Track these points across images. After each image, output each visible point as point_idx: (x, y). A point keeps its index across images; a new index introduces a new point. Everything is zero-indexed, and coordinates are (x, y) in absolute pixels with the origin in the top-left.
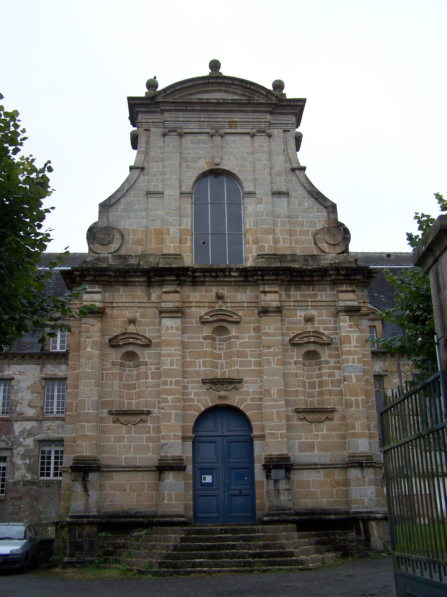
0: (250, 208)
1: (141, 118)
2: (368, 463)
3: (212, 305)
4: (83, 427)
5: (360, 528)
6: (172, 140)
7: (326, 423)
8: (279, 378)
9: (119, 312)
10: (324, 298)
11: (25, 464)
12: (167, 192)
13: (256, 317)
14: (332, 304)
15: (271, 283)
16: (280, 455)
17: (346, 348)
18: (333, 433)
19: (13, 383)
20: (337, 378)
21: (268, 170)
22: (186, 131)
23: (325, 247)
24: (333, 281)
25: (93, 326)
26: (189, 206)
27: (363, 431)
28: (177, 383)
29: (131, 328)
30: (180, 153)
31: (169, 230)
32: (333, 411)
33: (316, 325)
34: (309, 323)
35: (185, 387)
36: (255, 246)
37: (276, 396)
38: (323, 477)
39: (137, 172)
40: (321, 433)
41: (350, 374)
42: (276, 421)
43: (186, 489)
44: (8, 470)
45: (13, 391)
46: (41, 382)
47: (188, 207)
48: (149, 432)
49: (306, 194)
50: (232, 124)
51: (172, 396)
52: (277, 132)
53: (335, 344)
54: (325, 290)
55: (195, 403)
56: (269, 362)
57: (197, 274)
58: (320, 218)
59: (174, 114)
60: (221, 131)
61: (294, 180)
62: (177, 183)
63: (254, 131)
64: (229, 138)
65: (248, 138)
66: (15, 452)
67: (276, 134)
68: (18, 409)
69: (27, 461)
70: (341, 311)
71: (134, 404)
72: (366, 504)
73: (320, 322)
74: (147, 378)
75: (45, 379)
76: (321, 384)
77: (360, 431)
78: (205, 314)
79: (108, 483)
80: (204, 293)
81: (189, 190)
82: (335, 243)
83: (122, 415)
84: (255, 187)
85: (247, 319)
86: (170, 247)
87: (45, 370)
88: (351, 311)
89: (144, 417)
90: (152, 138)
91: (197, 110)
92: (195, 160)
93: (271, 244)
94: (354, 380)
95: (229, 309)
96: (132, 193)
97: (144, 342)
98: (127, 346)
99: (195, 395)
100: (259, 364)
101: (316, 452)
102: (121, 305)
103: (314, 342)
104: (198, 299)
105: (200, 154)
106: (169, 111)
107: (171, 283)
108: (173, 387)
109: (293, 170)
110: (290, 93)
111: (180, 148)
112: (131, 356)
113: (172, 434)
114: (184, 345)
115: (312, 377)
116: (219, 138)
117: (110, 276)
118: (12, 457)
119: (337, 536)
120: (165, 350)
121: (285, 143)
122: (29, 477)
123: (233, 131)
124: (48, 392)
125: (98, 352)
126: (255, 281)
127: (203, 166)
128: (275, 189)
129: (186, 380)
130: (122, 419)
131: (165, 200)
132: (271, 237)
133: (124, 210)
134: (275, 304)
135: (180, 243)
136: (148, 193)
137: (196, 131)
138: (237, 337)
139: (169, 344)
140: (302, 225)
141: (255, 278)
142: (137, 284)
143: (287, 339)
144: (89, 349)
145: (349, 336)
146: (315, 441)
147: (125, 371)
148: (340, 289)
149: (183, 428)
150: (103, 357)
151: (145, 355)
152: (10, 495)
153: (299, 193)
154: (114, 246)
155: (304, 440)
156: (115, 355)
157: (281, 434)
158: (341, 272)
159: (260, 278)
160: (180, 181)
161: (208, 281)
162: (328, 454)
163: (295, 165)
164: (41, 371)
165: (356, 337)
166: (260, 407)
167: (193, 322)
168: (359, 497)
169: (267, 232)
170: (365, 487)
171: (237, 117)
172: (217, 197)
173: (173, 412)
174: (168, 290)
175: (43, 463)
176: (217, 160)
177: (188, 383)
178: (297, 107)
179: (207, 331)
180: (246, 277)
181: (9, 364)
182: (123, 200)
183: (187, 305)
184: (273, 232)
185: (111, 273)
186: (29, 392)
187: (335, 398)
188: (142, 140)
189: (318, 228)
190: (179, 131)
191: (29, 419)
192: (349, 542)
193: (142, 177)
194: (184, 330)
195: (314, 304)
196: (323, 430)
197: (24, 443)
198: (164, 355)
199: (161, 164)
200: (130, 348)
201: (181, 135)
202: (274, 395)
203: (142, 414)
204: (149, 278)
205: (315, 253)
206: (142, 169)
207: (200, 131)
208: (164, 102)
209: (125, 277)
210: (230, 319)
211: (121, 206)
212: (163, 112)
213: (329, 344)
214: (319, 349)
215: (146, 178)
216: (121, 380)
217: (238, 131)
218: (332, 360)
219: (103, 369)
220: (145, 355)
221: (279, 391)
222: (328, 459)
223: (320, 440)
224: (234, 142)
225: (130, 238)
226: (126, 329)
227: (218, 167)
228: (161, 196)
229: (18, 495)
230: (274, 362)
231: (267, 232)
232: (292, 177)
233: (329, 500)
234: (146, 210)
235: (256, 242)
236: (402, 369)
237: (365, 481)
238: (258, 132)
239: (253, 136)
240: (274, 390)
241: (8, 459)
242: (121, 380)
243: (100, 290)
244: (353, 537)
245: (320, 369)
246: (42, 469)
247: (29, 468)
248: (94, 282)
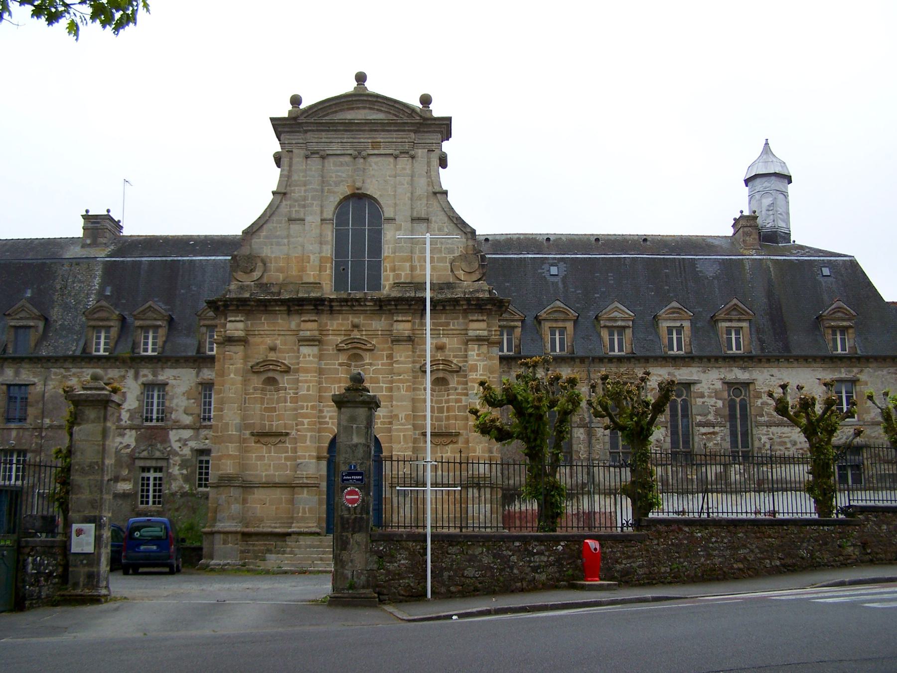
0: (389, 235)
1: (282, 137)
3: (348, 333)
4: (227, 447)
6: (315, 164)
7: (450, 446)
8: (407, 404)
9: (261, 340)
10: (456, 327)
11: (182, 474)
12: (309, 219)
13: (390, 344)
14: (463, 332)
15: (404, 312)
17: (472, 376)
19: (168, 388)
20: (464, 404)
21: (409, 195)
22: (328, 152)
23: (461, 274)
24: (465, 310)
25: (236, 353)
26: (330, 233)
28: (313, 407)
29: (272, 356)
30: (322, 177)
31: (308, 256)
32: (458, 434)
33: (447, 353)
34: (440, 351)
35: (321, 411)
36: (392, 274)
37: (404, 420)
39: (279, 197)
43: (320, 503)
44: (164, 481)
45: (167, 397)
46: (197, 387)
47: (329, 234)
48: (287, 452)
49: (446, 219)
50: (376, 145)
52: (421, 152)
53: (464, 371)
54: (457, 318)
55: (330, 425)
57: (333, 304)
59: (316, 134)
60: (364, 153)
61: (435, 204)
62: (318, 209)
63: (397, 152)
64: (373, 160)
65: (391, 160)
66: (171, 461)
67: (420, 154)
68: (173, 416)
69: (185, 472)
70: (471, 340)
71: (276, 425)
73: (450, 349)
74: (286, 402)
75: (201, 384)
76: (449, 409)
78: (341, 343)
79: (250, 497)
80: (340, 321)
81: (330, 216)
83: (264, 436)
84: (395, 212)
85: (381, 346)
86: (311, 276)
87: (201, 374)
88: (479, 340)
89: (282, 438)
90: (295, 160)
92: (337, 184)
93: (408, 272)
95: (364, 337)
96: (275, 218)
97: (283, 368)
98: (269, 373)
99: (330, 418)
100: (390, 389)
102: (262, 333)
103: (442, 370)
104: (335, 327)
105: (341, 176)
106: (313, 131)
107: (308, 312)
108: (309, 411)
109: (435, 193)
110: (437, 110)
111: (322, 171)
112: (272, 381)
113: (307, 454)
114: (321, 372)
115: (440, 402)
116: (362, 160)
117: (252, 306)
118: (168, 467)
120: (302, 376)
121: (429, 164)
122: (187, 487)
123: (376, 152)
124: (205, 398)
125: (240, 378)
126: (390, 310)
127: (344, 190)
128: (415, 215)
130: (263, 440)
131: (307, 227)
132: (408, 264)
133: (267, 237)
134: (407, 333)
135: (320, 271)
136: (291, 220)
137: (339, 152)
138: (371, 364)
139: (306, 371)
140: (441, 251)
141: (389, 307)
143: (418, 366)
144: (232, 376)
145: (476, 365)
147: (266, 395)
148: (471, 318)
149: (319, 449)
150: (246, 382)
151: (284, 381)
152: (168, 506)
153: (439, 218)
154: (256, 275)
156: (256, 381)
160: (322, 207)
163: (437, 189)
164: (198, 375)
166: (390, 430)
167: (330, 350)
169: (404, 260)
171: (380, 137)
172: (359, 220)
173: (309, 434)
174: (307, 319)
175: (201, 474)
176: (358, 184)
178: (444, 127)
179: (343, 358)
180: (381, 306)
181: (162, 368)
182: (265, 226)
183: (325, 333)
184: (411, 259)
185: (253, 303)
186: (184, 398)
187: (460, 423)
188: (285, 161)
189: (456, 255)
190: (322, 153)
191: (186, 427)
193: (284, 203)
194: (321, 357)
195: (446, 332)
197: (181, 453)
198: (302, 382)
199: (303, 188)
200: (271, 374)
201: (323, 158)
203: (280, 435)
204: (289, 306)
205: (451, 281)
206: (285, 194)
207: (343, 152)
208: (306, 123)
210: (364, 347)
211: (264, 233)
212: (306, 132)
213: (458, 372)
214: (448, 376)
215: (288, 203)
216: (262, 403)
217: (382, 152)
218: (460, 387)
219: (246, 394)
220: (284, 381)
221: (407, 416)
224: (376, 163)
225: (272, 266)
226: (267, 356)
227: (359, 191)
228: (302, 222)
229: (177, 506)
231: (404, 260)
232: (434, 202)
234: (288, 236)
235: (393, 269)
236: (592, 376)
239: (396, 157)
240: (402, 415)
241: (164, 469)
242: (262, 403)
243: (242, 319)
245: (448, 395)
246: (200, 479)
247: (187, 479)
248: (237, 311)
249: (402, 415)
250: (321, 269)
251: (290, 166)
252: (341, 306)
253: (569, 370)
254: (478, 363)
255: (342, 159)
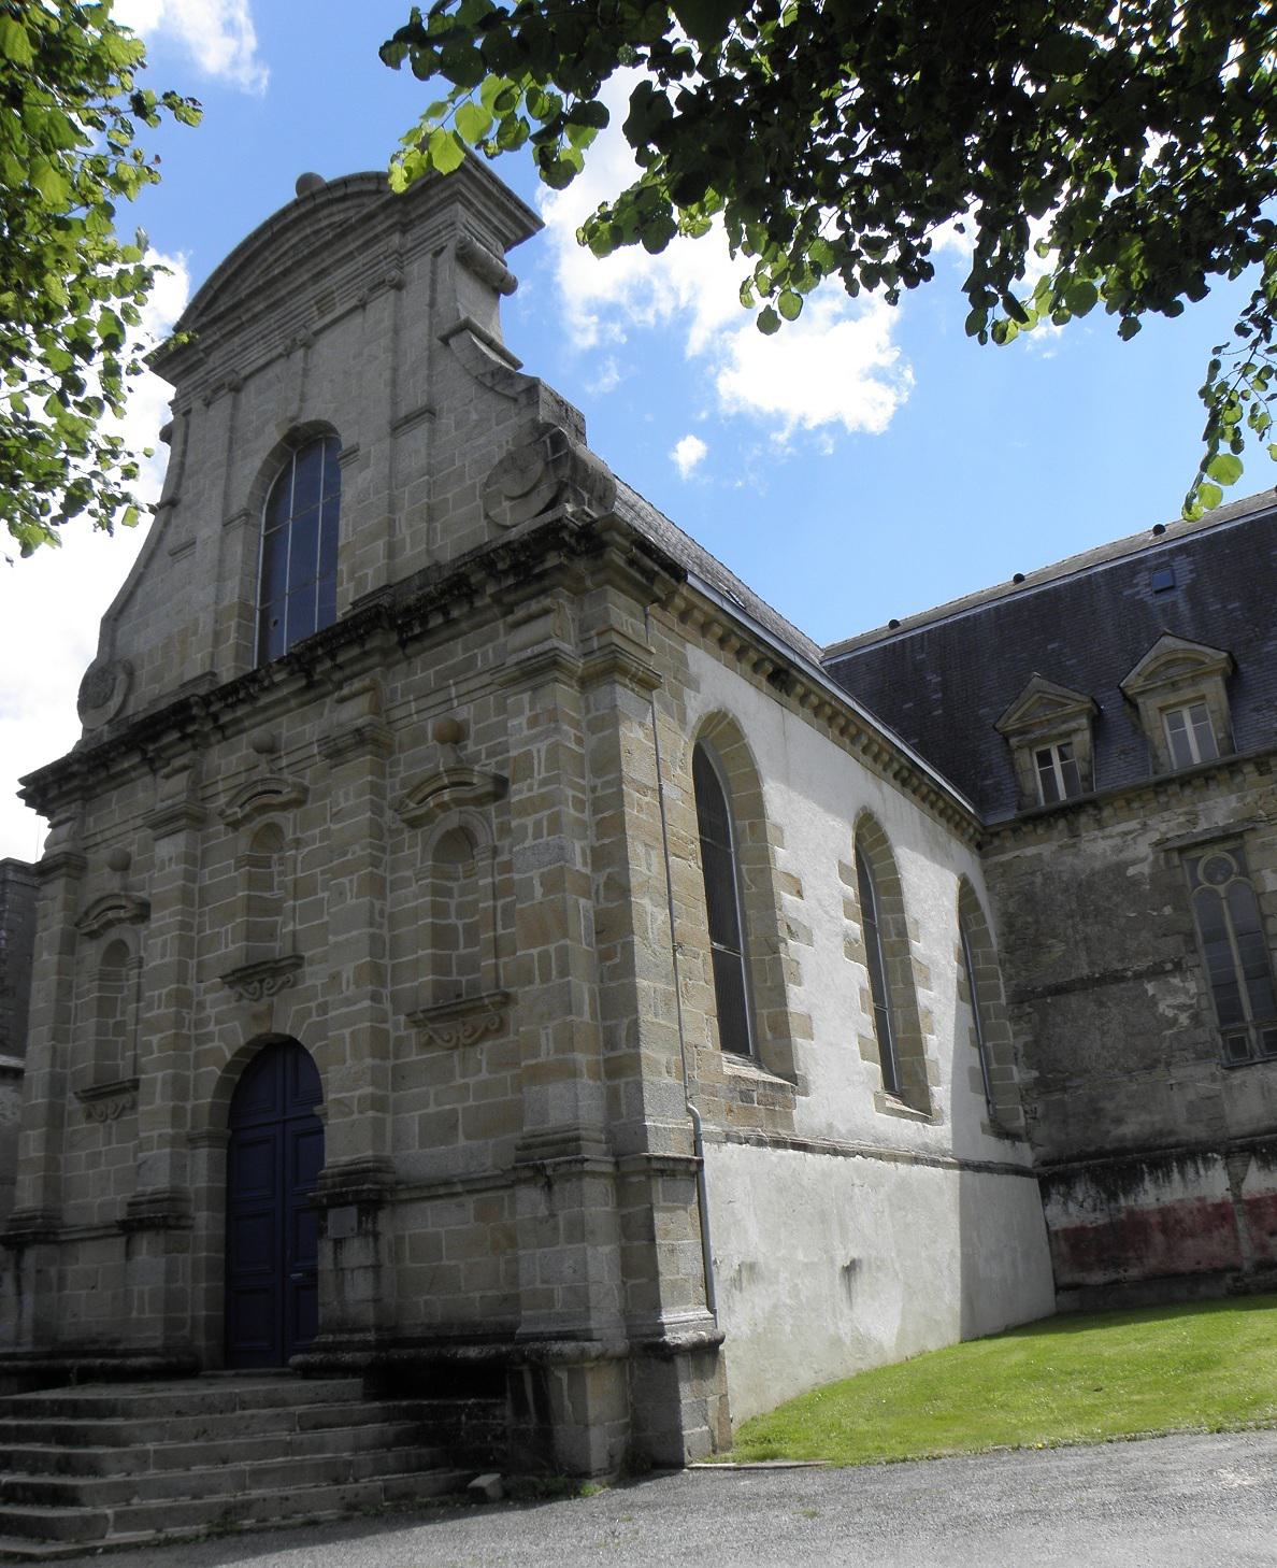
2: (559, 1164)
5: (523, 1392)
7: (488, 1044)
16: (352, 1163)
18: (504, 1074)
21: (387, 375)
27: (561, 1056)
38: (472, 1220)
39: (163, 513)
40: (476, 1078)
41: (528, 875)
42: (349, 1062)
50: (324, 303)
51: (160, 1035)
56: (341, 894)
58: (500, 434)
72: (558, 1307)
77: (553, 1057)
82: (526, 490)
91: (262, 312)
94: (539, 891)
101: (462, 1142)
119: (463, 1418)
123: (328, 319)
129: (202, 985)
137: (262, 362)
142: (133, 774)
146: (459, 1106)
155: (432, 1109)
157: (359, 1100)
158: (501, 566)
159: (328, 664)
161: (248, 715)
162: (491, 1142)
165: (547, 751)
168: (538, 1285)
170: (558, 1248)
177: (205, 993)
188: (178, 436)
192: (495, 1437)
196: (480, 1071)
202: (348, 986)
209: (106, 766)
222: (489, 1162)
223: (471, 1102)
230: (351, 890)
233: (489, 1293)
237: (556, 1228)
238: (372, 290)
244: (506, 1423)
249: (348, 972)
250: (1111, 837)
251: (186, 442)
252: (232, 706)
253: (1233, 801)
254: (534, 748)
255: (270, 373)
